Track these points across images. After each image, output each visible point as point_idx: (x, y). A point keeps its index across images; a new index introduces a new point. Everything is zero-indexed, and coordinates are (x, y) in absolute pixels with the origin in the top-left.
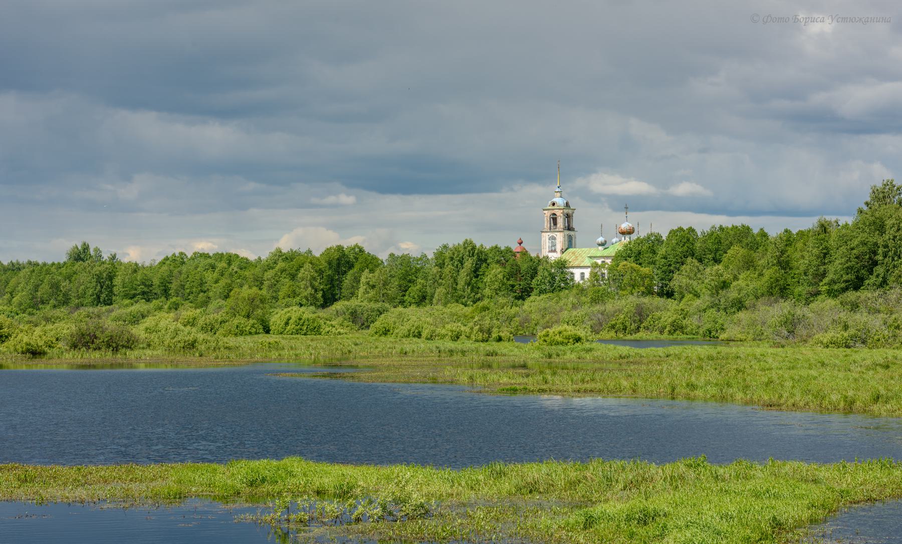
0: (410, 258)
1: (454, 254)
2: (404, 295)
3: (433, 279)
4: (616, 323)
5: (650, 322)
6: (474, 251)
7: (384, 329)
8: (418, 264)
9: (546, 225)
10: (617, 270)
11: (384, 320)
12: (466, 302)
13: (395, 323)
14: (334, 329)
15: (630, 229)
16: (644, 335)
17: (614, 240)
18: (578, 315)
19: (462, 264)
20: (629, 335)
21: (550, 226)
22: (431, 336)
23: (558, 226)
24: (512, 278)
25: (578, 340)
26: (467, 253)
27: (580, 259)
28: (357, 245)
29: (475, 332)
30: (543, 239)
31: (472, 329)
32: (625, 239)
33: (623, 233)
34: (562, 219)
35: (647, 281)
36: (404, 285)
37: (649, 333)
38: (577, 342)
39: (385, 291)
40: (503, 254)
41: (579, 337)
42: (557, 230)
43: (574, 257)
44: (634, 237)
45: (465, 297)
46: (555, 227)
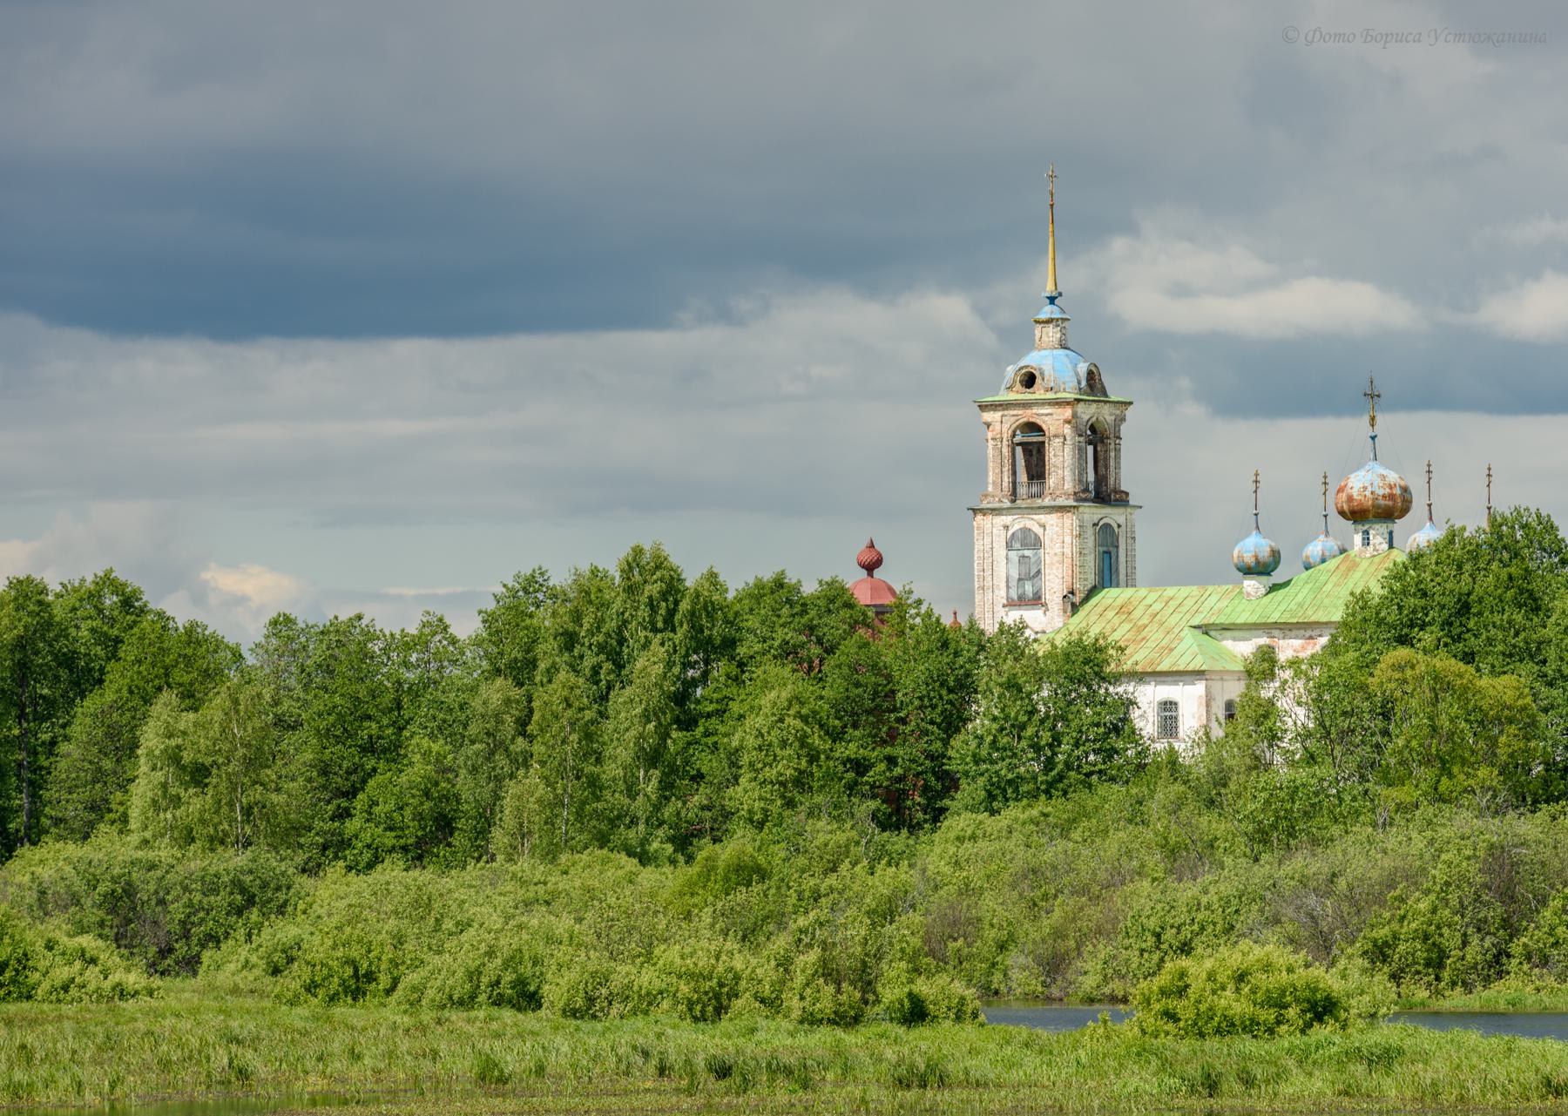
0: (370, 636)
1: (577, 617)
2: (344, 814)
3: (488, 734)
4: (1395, 937)
5: (1552, 928)
6: (676, 603)
7: (349, 971)
8: (406, 664)
9: (995, 478)
10: (1363, 687)
11: (348, 930)
12: (644, 842)
13: (399, 940)
14: (92, 973)
15: (1391, 497)
16: (1530, 988)
17: (1314, 549)
18: (1204, 900)
19: (620, 666)
20: (1459, 989)
21: (1014, 483)
22: (591, 1000)
23: (1051, 481)
24: (855, 726)
25: (1322, 1009)
26: (644, 613)
27: (1155, 636)
28: (107, 581)
29: (799, 980)
30: (978, 546)
31: (785, 964)
32: (1366, 542)
33: (1357, 515)
34: (1068, 449)
35: (1507, 741)
36: (345, 764)
37: (1551, 981)
38: (1319, 1018)
39: (256, 794)
40: (812, 613)
41: (1328, 998)
42: (1047, 501)
43: (1126, 626)
44: (1420, 534)
45: (634, 822)
46: (1034, 489)
